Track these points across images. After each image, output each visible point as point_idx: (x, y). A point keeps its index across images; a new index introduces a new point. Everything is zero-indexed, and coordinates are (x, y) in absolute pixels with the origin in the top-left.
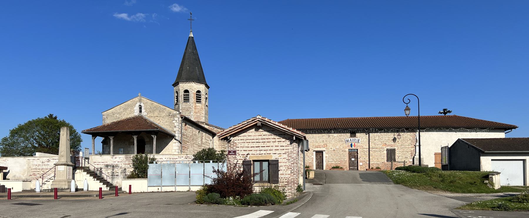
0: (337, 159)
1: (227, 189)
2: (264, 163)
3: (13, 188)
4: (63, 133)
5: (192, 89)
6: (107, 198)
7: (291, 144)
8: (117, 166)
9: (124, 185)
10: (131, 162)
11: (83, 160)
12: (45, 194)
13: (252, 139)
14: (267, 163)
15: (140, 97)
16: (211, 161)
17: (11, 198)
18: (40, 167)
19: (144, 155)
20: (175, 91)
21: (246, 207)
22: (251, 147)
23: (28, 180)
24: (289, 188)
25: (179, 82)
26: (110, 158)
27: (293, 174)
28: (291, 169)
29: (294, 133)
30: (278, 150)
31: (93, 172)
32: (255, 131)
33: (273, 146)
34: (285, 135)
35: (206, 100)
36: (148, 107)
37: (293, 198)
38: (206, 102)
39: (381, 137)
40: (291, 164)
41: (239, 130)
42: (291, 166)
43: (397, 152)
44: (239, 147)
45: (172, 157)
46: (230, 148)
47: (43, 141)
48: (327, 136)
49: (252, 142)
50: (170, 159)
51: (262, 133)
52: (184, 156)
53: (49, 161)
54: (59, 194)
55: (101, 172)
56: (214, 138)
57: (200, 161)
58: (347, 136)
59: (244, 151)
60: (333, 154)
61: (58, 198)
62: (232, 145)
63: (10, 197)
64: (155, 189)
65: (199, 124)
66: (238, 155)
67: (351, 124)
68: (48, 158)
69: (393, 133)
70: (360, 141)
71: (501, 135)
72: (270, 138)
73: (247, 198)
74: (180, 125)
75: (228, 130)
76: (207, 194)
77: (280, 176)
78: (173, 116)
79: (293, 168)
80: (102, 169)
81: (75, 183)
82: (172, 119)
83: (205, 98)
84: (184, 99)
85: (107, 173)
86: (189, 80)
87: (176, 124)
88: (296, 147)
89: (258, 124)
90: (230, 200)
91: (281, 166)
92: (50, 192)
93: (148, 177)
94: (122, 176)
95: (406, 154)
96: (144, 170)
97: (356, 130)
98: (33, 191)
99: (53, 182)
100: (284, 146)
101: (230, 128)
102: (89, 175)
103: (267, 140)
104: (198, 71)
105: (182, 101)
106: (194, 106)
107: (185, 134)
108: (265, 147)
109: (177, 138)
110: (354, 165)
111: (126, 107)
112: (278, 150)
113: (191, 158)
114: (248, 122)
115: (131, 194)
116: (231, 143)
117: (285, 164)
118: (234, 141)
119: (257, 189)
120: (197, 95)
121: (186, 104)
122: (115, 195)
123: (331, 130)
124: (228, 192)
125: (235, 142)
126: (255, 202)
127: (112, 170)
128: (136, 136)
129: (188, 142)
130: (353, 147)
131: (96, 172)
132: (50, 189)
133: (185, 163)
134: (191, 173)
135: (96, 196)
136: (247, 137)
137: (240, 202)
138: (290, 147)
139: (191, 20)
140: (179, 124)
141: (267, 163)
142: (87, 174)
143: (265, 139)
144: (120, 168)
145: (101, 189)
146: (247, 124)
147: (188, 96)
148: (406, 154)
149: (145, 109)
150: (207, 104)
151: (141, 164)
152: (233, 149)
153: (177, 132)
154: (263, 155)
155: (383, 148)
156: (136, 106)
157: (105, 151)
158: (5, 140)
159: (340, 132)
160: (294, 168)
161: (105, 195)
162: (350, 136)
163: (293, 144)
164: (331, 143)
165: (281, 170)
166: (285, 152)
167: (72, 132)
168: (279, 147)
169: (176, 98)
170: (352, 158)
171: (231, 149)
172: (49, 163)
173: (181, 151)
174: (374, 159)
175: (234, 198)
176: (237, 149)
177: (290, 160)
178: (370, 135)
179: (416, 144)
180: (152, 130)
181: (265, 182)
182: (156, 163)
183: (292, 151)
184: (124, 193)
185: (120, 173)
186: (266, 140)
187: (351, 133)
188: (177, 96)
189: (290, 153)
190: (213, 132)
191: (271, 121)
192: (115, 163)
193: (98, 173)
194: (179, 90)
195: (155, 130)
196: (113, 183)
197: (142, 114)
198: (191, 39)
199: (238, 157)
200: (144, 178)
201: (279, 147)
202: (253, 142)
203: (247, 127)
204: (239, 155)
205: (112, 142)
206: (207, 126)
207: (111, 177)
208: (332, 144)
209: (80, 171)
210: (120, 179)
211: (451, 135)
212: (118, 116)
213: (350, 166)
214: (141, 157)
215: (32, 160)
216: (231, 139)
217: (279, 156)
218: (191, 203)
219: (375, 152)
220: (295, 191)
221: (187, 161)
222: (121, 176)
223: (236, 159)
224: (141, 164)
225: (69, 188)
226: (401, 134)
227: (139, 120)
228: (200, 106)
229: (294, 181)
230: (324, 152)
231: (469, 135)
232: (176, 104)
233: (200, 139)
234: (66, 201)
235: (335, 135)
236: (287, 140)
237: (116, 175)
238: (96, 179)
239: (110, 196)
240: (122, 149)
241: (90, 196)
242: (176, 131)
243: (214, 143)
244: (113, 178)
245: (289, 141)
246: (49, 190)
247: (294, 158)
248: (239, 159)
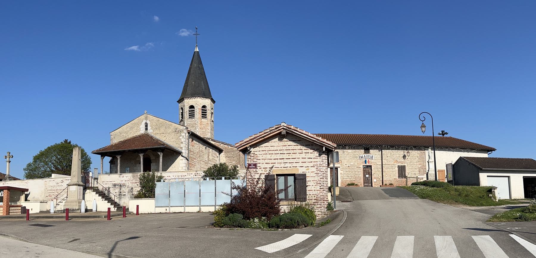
0: (352, 176)
1: (251, 208)
2: (289, 177)
3: (32, 209)
5: (198, 105)
6: (115, 219)
7: (320, 155)
8: (124, 185)
9: (132, 205)
10: (138, 180)
11: (93, 180)
12: (58, 215)
13: (275, 150)
14: (293, 177)
16: (223, 178)
17: (30, 219)
18: (55, 188)
19: (151, 173)
20: (180, 107)
21: (276, 230)
22: (274, 159)
23: (45, 201)
24: (318, 206)
25: (184, 98)
27: (323, 190)
28: (320, 184)
29: (324, 143)
30: (305, 162)
31: (102, 192)
32: (278, 140)
33: (299, 158)
34: (313, 145)
35: (212, 115)
36: (154, 124)
37: (323, 219)
38: (212, 117)
39: (392, 154)
40: (321, 178)
41: (261, 139)
42: (320, 181)
43: (407, 169)
44: (260, 159)
45: (180, 174)
46: (250, 160)
47: (59, 165)
48: (341, 152)
49: (275, 154)
50: (179, 176)
51: (287, 143)
52: (194, 173)
53: (62, 182)
54: (70, 215)
55: (109, 191)
56: (220, 155)
57: (211, 178)
58: (361, 152)
59: (266, 163)
60: (348, 171)
61: (69, 219)
62: (252, 158)
63: (29, 218)
64: (163, 210)
65: (207, 140)
66: (260, 168)
67: (364, 141)
68: (62, 179)
69: (403, 151)
70: (373, 158)
71: (485, 155)
72: (296, 149)
73: (275, 219)
74: (187, 140)
75: (248, 139)
76: (227, 215)
77: (308, 193)
78: (179, 132)
79: (322, 183)
80: (110, 189)
81: (85, 203)
82: (179, 135)
83: (210, 113)
84: (189, 115)
85: (114, 193)
86: (194, 95)
87: (183, 140)
88: (325, 159)
89: (282, 132)
90: (255, 222)
91: (309, 181)
92: (63, 213)
93: (156, 197)
94: (129, 196)
95: (414, 171)
96: (151, 189)
97: (370, 147)
98: (48, 212)
99: (65, 202)
100: (312, 158)
101: (250, 137)
102: (98, 195)
103: (292, 152)
104: (203, 86)
105: (187, 117)
106: (199, 122)
107: (192, 150)
108: (290, 159)
109: (184, 155)
110: (368, 182)
111: (133, 126)
112: (305, 162)
113: (201, 175)
114: (271, 131)
115: (138, 215)
116: (251, 155)
117: (313, 178)
118: (254, 152)
119: (284, 208)
120: (202, 110)
121: (192, 120)
122: (123, 216)
123: (345, 146)
124: (251, 212)
125: (256, 154)
126: (286, 223)
127: (119, 190)
128: (143, 154)
129: (195, 159)
130: (367, 163)
131: (104, 191)
132: (63, 209)
133: (194, 180)
134: (201, 192)
135: (105, 217)
136: (269, 147)
137: (267, 224)
138: (319, 159)
139: (196, 34)
140: (186, 140)
141: (293, 177)
142: (96, 194)
143: (290, 150)
144: (126, 187)
145: (109, 209)
146: (270, 132)
147: (194, 112)
148: (414, 171)
150: (213, 119)
151: (148, 182)
152: (253, 162)
153: (184, 148)
154: (289, 168)
155: (395, 165)
157: (113, 171)
158: (29, 165)
159: (354, 149)
160: (323, 184)
161: (113, 216)
162: (364, 152)
163: (322, 155)
164: (346, 159)
165: (309, 186)
166: (314, 165)
167: (83, 155)
168: (307, 159)
169: (181, 115)
170: (367, 174)
171: (251, 162)
173: (188, 169)
174: (386, 176)
175: (260, 219)
176: (258, 162)
177: (319, 174)
178: (383, 152)
179: (429, 160)
180: (159, 147)
181: (290, 200)
182: (164, 181)
183: (321, 164)
184: (131, 214)
185: (127, 192)
186: (291, 151)
187: (365, 149)
188: (182, 113)
189: (318, 166)
190: (220, 148)
191: (298, 130)
192: (123, 182)
193: (106, 192)
194: (184, 106)
195: (162, 146)
196: (121, 203)
197: (148, 132)
198: (197, 54)
199: (259, 171)
200: (151, 198)
201: (307, 159)
202: (276, 154)
203: (270, 136)
204: (261, 168)
205: (119, 161)
206: (213, 142)
207: (118, 197)
208: (346, 160)
209: (90, 191)
210: (127, 199)
211: (449, 154)
212: (124, 135)
213: (364, 183)
214: (149, 175)
215: (48, 182)
216: (251, 150)
217: (306, 170)
218: (209, 226)
219: (387, 168)
220: (325, 210)
221: (197, 179)
222: (128, 196)
223: (257, 173)
224: (148, 182)
225: (79, 209)
226: (410, 151)
227: (145, 137)
229: (324, 198)
230: (338, 168)
231: (463, 155)
232: (181, 121)
233: (207, 156)
234: (74, 222)
235: (350, 151)
236: (316, 151)
237: (124, 195)
238: (104, 199)
239: (117, 217)
240: (128, 169)
241: (99, 217)
242: (183, 147)
243: (221, 160)
244: (120, 198)
245: (317, 152)
246: (62, 210)
247: (323, 172)
248: (260, 173)
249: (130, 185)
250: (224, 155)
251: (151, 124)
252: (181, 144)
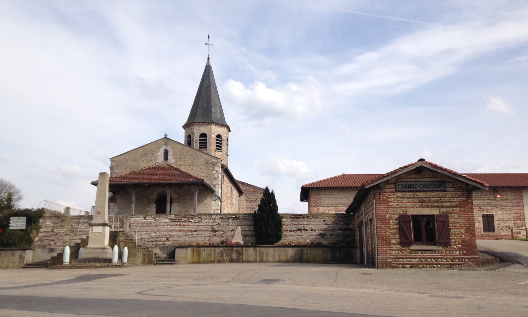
78: (212, 165)
82: (211, 168)
149: (174, 154)
156: (160, 151)
194: (193, 133)
197: (169, 162)
228: (221, 155)
250: (244, 199)
252: (214, 181)
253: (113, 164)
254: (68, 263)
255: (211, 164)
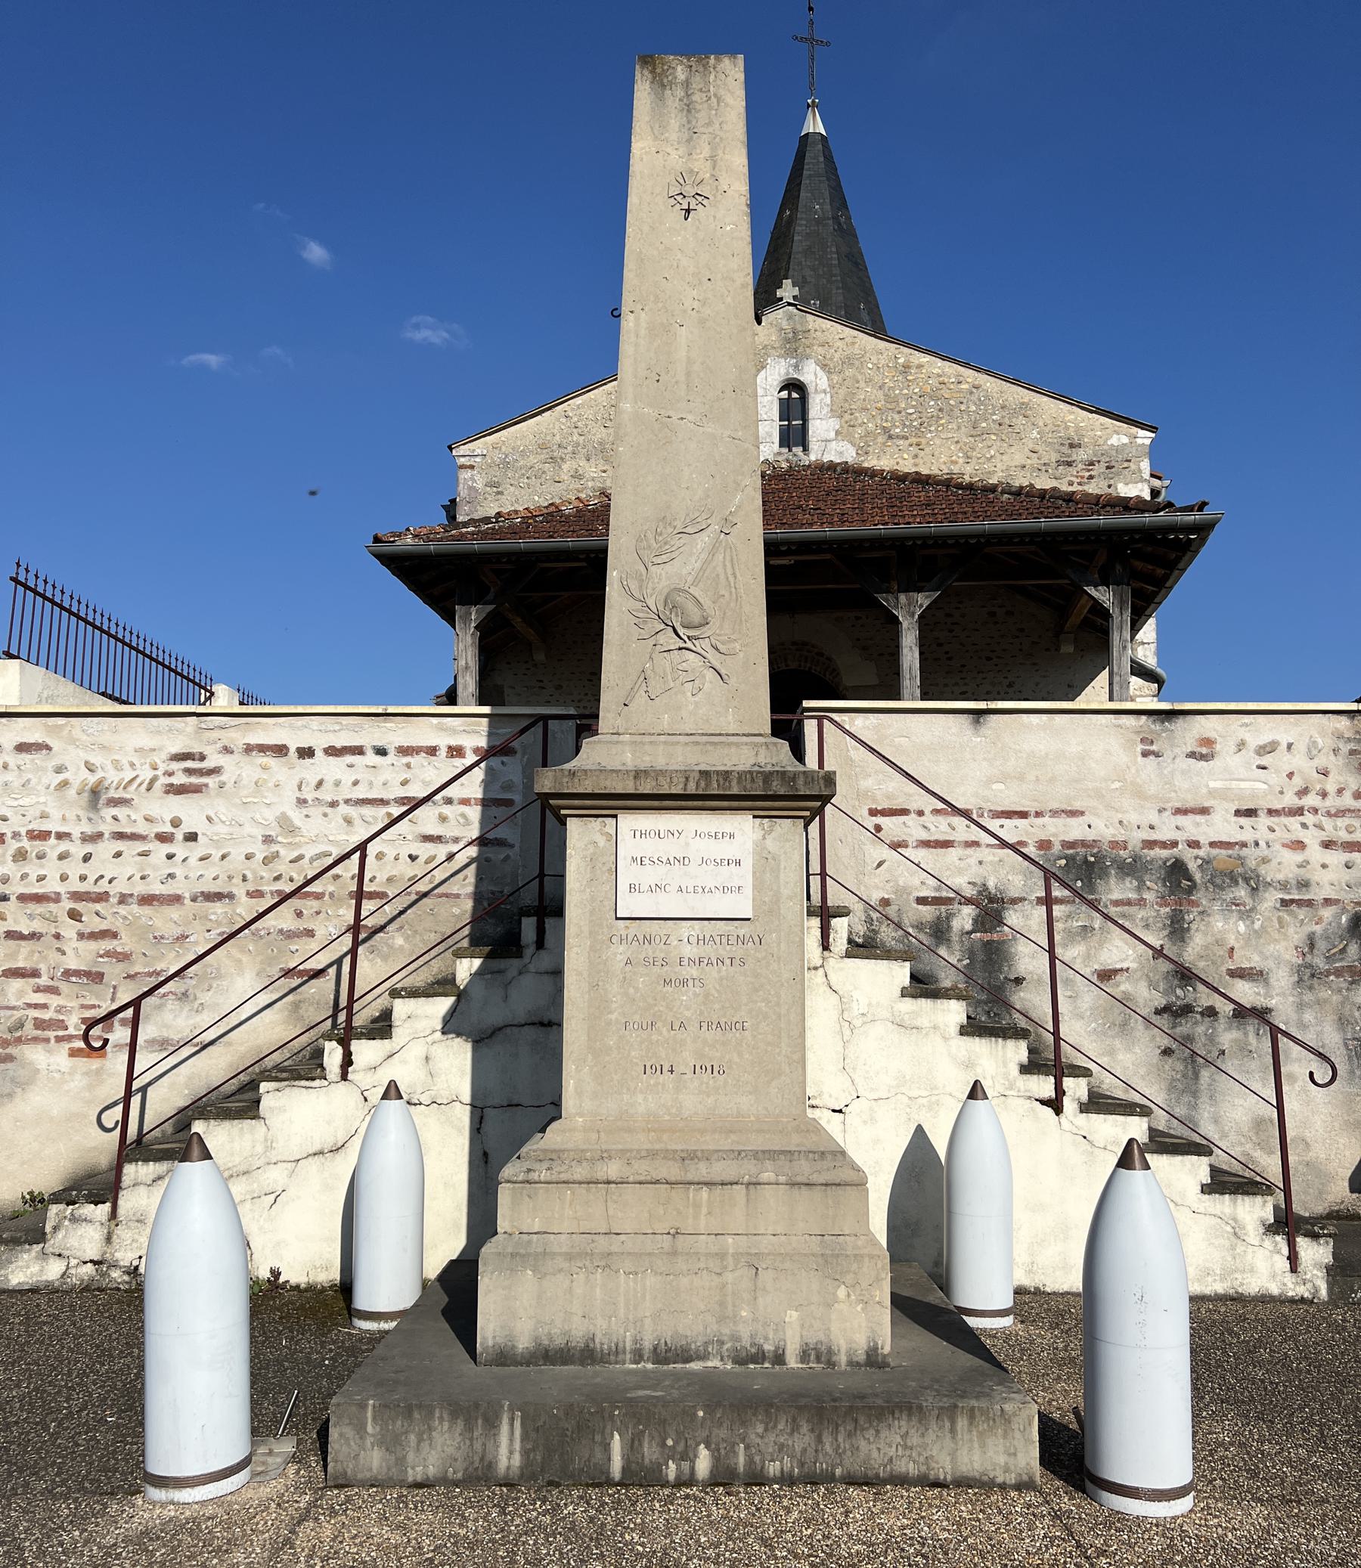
4: (675, 158)
15: (790, 317)
26: (1122, 757)
78: (1097, 470)
139: (811, 40)
144: (1271, 898)
172: (190, 812)
185: (1282, 979)
249: (1317, 876)
251: (842, 392)
253: (472, 479)
254: (1007, 1321)
255: (1092, 464)
